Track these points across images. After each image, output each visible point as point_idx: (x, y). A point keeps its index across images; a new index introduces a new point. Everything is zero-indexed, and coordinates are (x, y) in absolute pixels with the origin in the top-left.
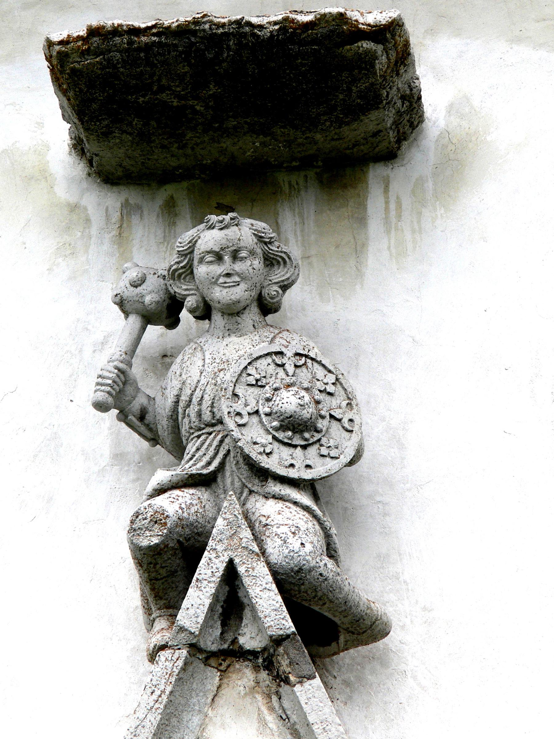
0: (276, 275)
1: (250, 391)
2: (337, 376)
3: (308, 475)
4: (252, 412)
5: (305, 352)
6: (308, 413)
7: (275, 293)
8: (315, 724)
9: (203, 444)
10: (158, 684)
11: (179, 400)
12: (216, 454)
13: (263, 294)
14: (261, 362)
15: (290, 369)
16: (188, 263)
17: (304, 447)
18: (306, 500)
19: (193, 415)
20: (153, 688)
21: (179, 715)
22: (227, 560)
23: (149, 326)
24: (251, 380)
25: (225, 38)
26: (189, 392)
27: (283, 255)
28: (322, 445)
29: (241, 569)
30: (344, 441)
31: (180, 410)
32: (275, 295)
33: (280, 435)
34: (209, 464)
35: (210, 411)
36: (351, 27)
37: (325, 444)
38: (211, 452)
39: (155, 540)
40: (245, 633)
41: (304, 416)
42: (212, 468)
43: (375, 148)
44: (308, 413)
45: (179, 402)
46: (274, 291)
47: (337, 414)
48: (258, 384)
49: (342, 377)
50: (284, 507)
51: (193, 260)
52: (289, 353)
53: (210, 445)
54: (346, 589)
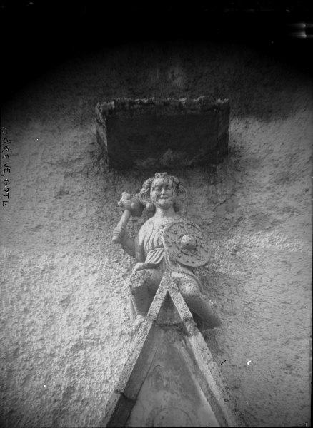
3: (193, 265)
12: (159, 258)
15: (186, 228)
17: (192, 256)
18: (190, 273)
19: (150, 245)
24: (172, 231)
25: (301, 30)
26: (142, 239)
29: (172, 295)
31: (145, 243)
33: (184, 251)
34: (157, 261)
38: (158, 257)
39: (139, 285)
42: (157, 262)
47: (202, 245)
48: (175, 233)
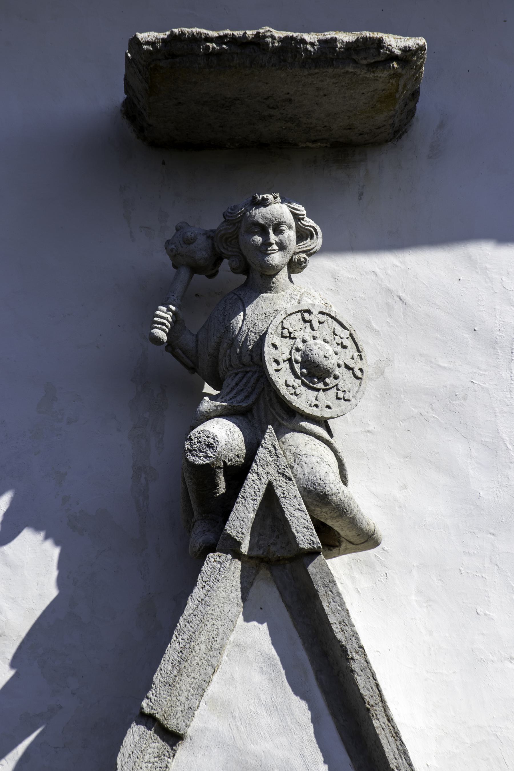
0: (305, 244)
1: (284, 341)
2: (350, 332)
4: (286, 359)
5: (327, 311)
6: (331, 363)
7: (303, 260)
8: (334, 624)
9: (240, 381)
10: (208, 581)
11: (221, 341)
13: (293, 259)
14: (293, 318)
16: (235, 230)
20: (204, 584)
21: (221, 606)
22: (267, 482)
23: (195, 275)
27: (311, 229)
28: (338, 389)
29: (279, 492)
30: (355, 387)
32: (303, 261)
35: (249, 355)
36: (386, 50)
37: (341, 389)
40: (276, 543)
41: (328, 366)
43: (376, 137)
44: (331, 363)
45: (221, 343)
46: (302, 258)
49: (355, 333)
50: (309, 439)
51: (240, 228)
52: (315, 311)
53: (248, 382)
54: (355, 510)
